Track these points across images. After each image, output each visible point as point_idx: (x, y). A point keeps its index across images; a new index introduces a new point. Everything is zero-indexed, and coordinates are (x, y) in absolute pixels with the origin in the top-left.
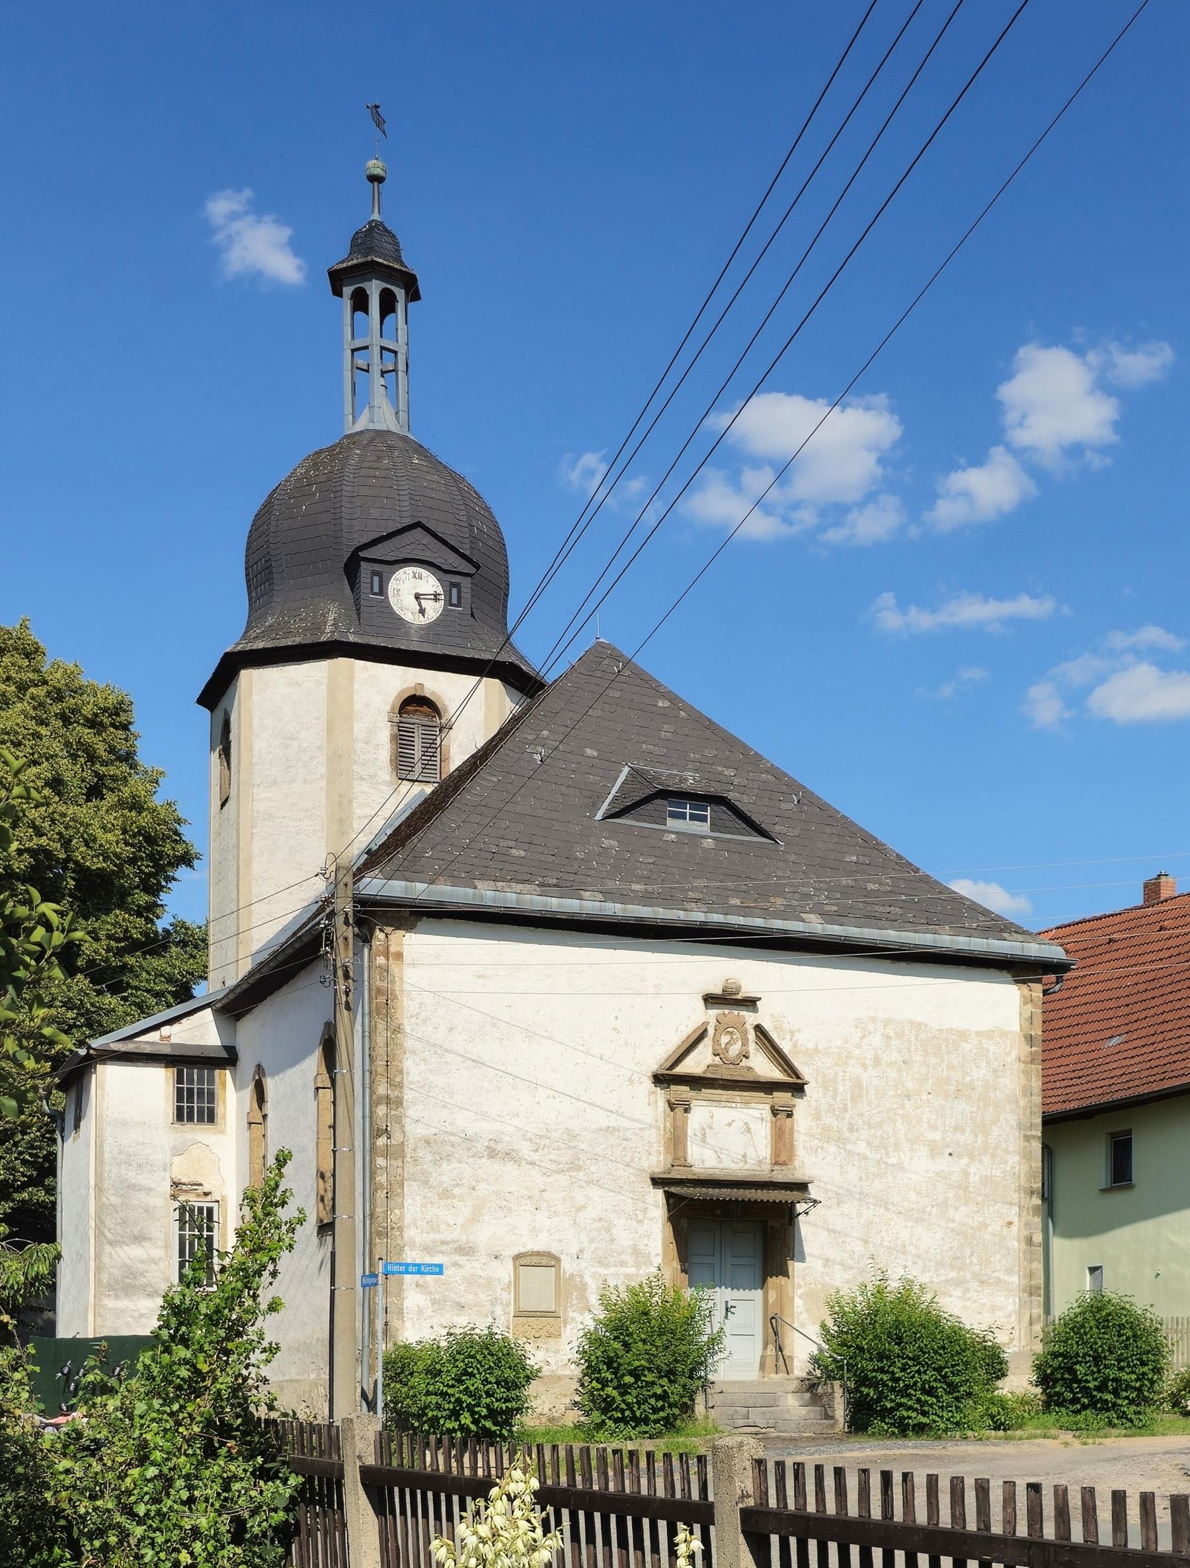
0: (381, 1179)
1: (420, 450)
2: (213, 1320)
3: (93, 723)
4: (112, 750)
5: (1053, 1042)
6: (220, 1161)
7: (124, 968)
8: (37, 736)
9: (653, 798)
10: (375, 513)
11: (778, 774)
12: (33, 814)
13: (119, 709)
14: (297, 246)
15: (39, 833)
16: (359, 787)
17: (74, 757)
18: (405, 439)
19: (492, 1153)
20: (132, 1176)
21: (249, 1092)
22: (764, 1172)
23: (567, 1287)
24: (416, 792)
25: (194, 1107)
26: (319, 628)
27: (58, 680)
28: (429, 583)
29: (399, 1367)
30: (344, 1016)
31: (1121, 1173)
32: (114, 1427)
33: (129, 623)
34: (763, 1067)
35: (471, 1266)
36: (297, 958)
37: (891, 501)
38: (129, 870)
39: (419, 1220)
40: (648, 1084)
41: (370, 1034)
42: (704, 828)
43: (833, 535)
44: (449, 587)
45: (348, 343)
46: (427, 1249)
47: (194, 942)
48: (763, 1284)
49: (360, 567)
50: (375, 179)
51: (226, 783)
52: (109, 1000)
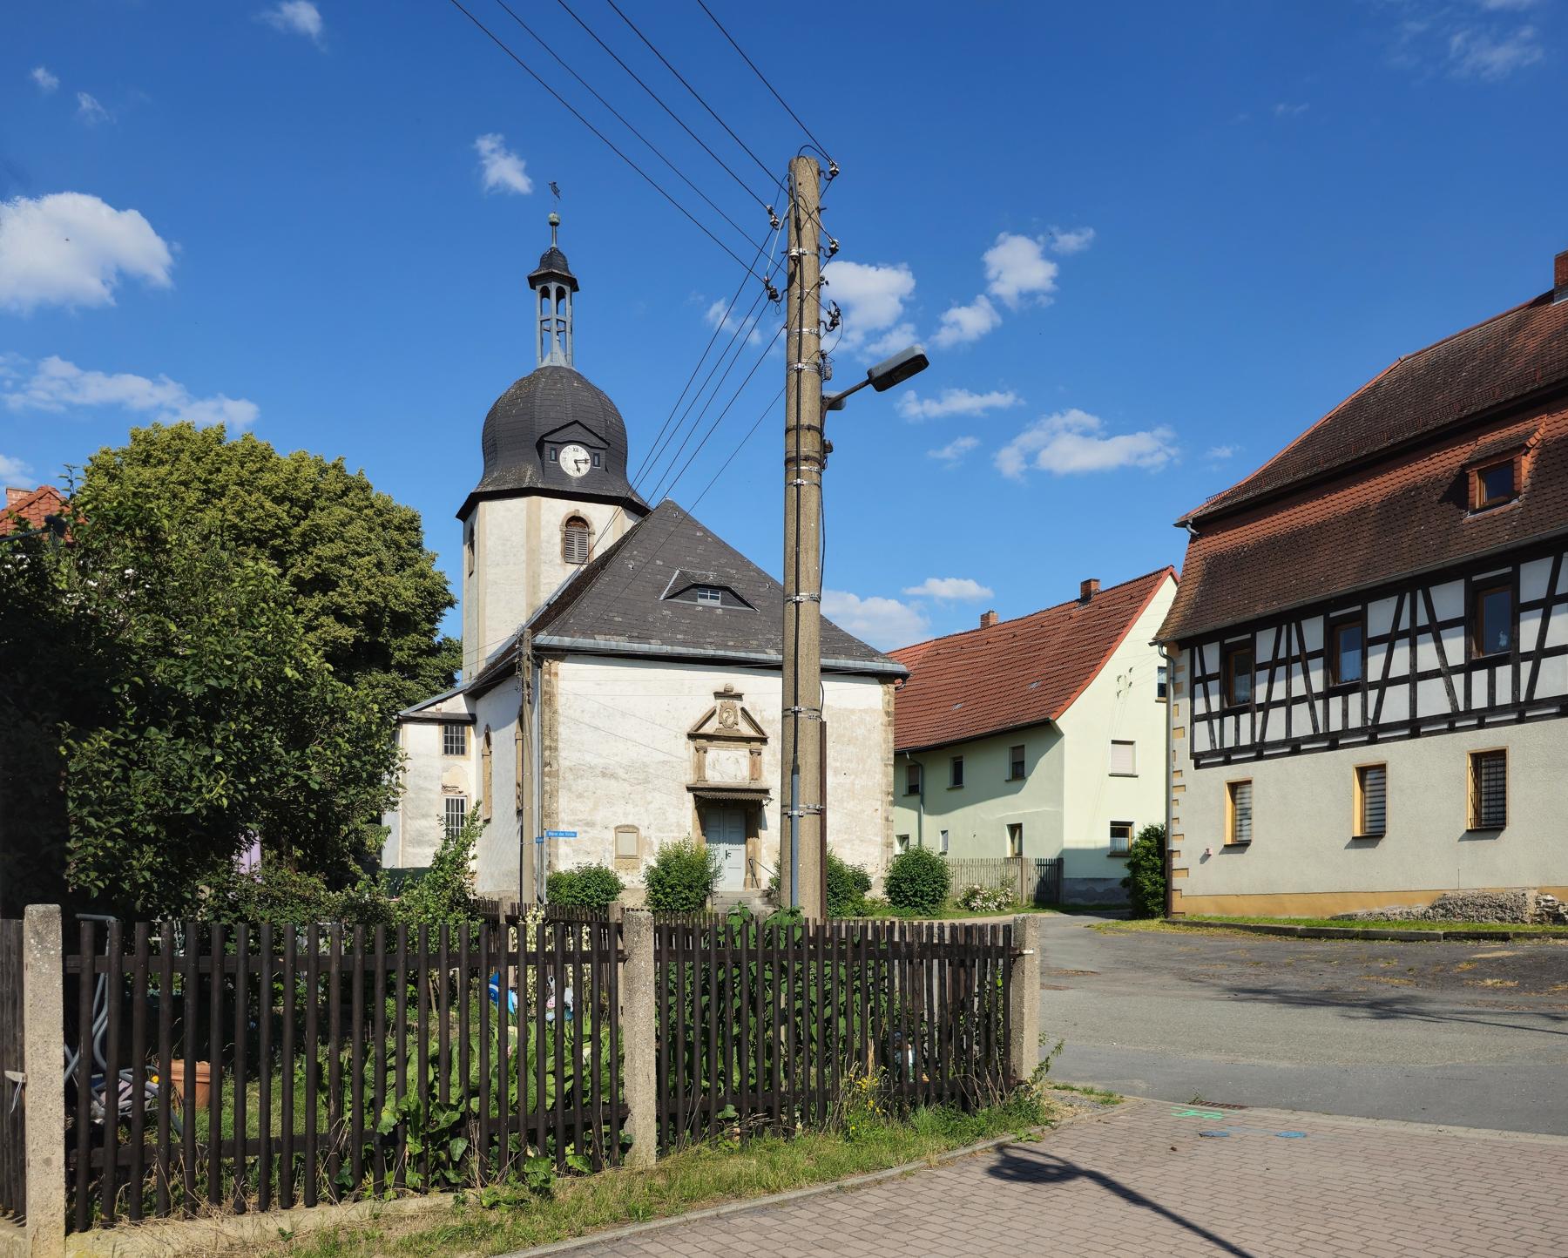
0: (547, 788)
1: (579, 377)
2: (452, 862)
3: (398, 528)
4: (409, 543)
5: (900, 716)
6: (467, 774)
7: (417, 665)
8: (369, 539)
9: (690, 588)
10: (552, 415)
11: (759, 572)
12: (367, 583)
13: (413, 519)
14: (527, 171)
15: (370, 592)
16: (544, 568)
17: (389, 548)
18: (570, 371)
19: (604, 775)
20: (421, 783)
21: (482, 738)
22: (746, 784)
23: (642, 843)
24: (571, 570)
25: (454, 746)
26: (522, 479)
27: (379, 504)
28: (582, 454)
29: (555, 884)
30: (527, 707)
31: (958, 780)
32: (416, 900)
33: (417, 470)
34: (745, 730)
35: (593, 832)
36: (502, 672)
37: (909, 327)
38: (419, 611)
39: (567, 809)
40: (685, 739)
41: (542, 714)
42: (717, 603)
43: (874, 349)
44: (593, 456)
45: (539, 318)
46: (570, 824)
47: (455, 649)
48: (745, 842)
49: (545, 445)
50: (554, 224)
51: (472, 563)
52: (409, 683)
